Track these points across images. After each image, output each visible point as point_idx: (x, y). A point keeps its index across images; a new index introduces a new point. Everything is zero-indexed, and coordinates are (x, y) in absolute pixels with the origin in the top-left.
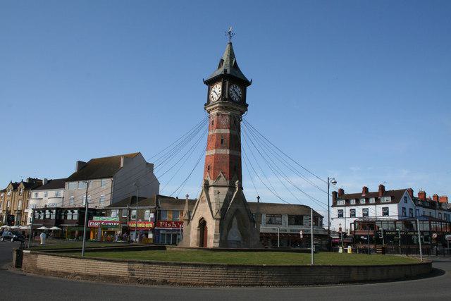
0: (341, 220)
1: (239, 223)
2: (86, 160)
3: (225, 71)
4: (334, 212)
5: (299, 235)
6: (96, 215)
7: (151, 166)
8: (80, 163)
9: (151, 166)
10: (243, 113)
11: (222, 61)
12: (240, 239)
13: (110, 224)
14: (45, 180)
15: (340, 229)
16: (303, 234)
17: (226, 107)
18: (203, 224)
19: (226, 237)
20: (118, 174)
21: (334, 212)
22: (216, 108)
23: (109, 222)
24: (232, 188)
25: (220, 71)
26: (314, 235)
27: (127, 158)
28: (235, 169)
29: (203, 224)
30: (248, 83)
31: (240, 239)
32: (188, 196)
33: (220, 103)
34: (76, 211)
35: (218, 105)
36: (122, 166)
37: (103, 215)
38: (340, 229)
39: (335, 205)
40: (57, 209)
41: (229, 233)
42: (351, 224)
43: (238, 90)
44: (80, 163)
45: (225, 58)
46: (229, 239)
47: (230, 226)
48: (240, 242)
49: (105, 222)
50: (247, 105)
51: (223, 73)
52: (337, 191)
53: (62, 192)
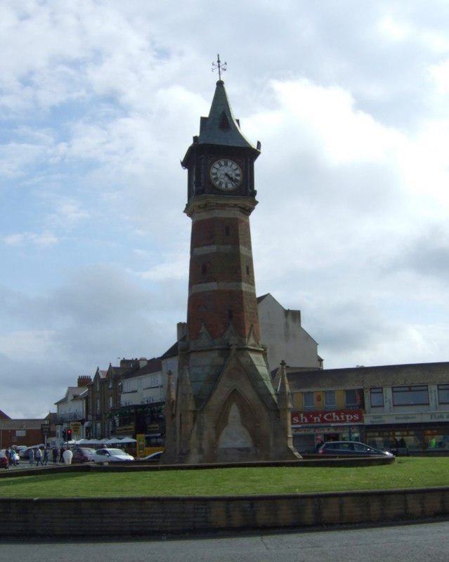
1: (243, 413)
12: (249, 444)
19: (214, 445)
28: (231, 317)
48: (247, 450)
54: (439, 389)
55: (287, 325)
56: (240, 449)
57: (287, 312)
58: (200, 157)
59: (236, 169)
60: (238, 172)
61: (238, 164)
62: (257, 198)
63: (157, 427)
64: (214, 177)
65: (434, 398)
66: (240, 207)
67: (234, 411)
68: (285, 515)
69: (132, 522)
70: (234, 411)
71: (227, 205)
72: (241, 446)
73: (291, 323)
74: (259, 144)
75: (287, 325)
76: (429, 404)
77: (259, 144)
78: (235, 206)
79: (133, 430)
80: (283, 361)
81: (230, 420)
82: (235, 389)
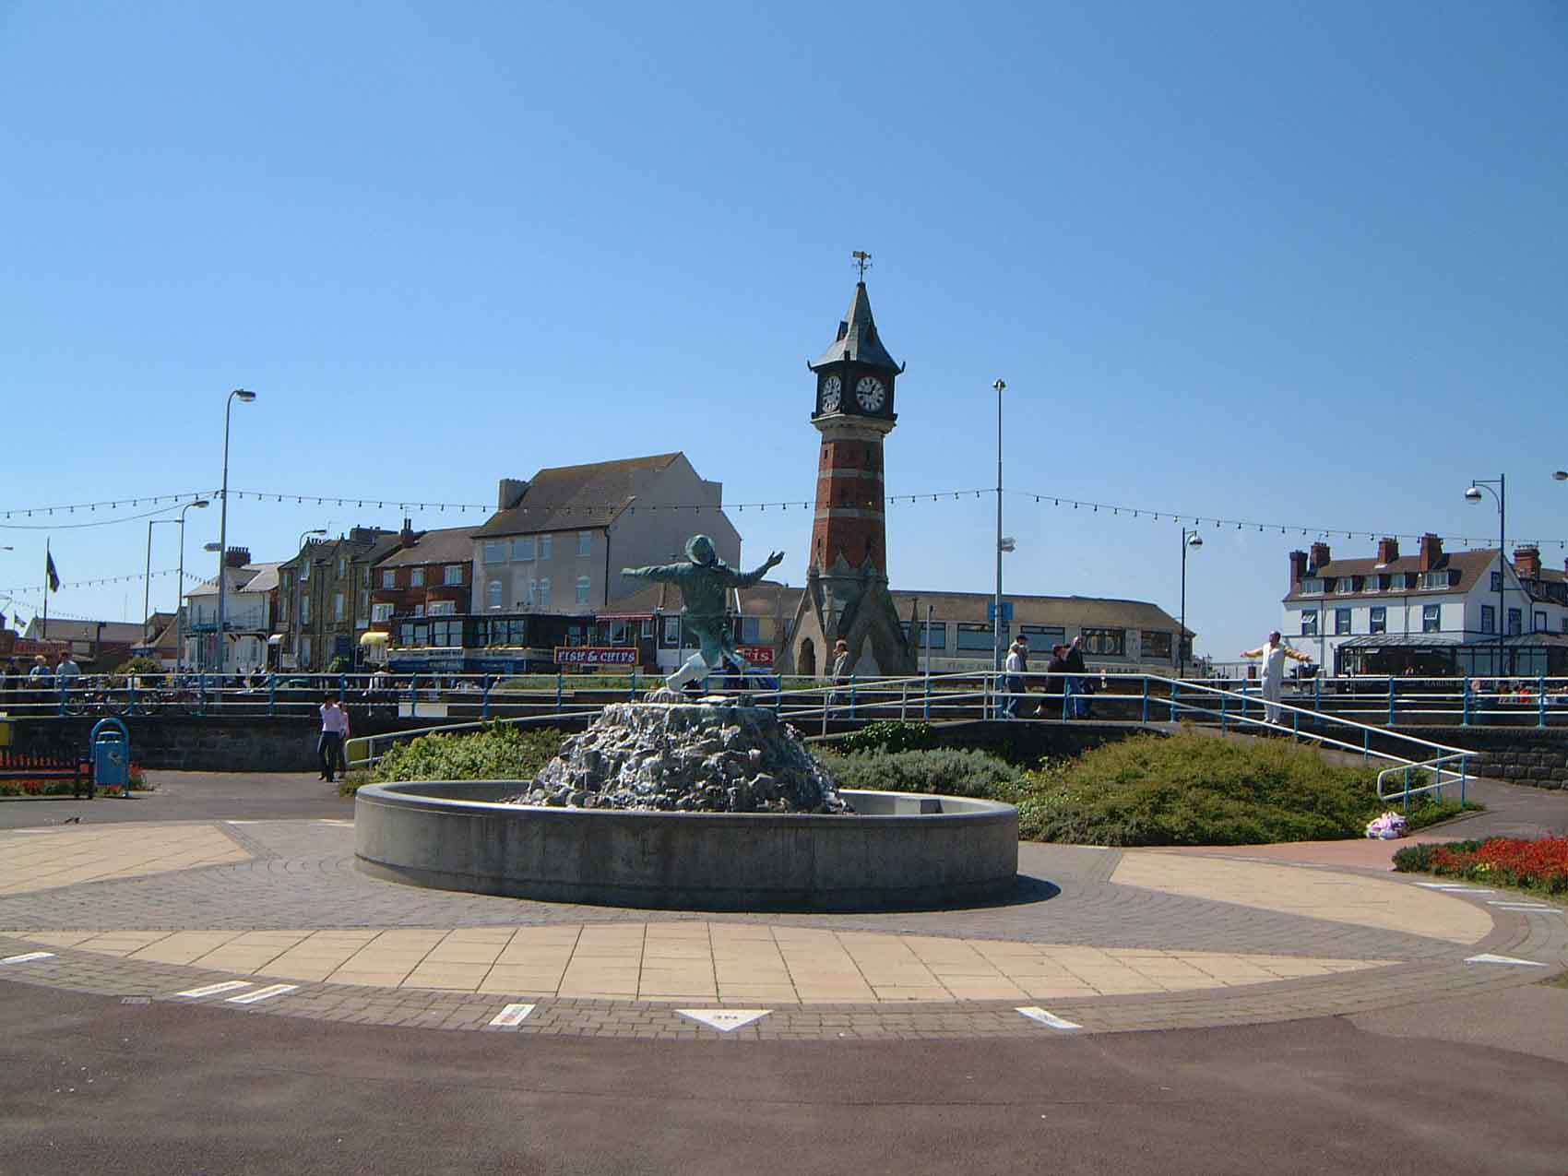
2: (526, 476)
7: (714, 490)
10: (884, 432)
54: (958, 630)
59: (881, 396)
67: (868, 643)
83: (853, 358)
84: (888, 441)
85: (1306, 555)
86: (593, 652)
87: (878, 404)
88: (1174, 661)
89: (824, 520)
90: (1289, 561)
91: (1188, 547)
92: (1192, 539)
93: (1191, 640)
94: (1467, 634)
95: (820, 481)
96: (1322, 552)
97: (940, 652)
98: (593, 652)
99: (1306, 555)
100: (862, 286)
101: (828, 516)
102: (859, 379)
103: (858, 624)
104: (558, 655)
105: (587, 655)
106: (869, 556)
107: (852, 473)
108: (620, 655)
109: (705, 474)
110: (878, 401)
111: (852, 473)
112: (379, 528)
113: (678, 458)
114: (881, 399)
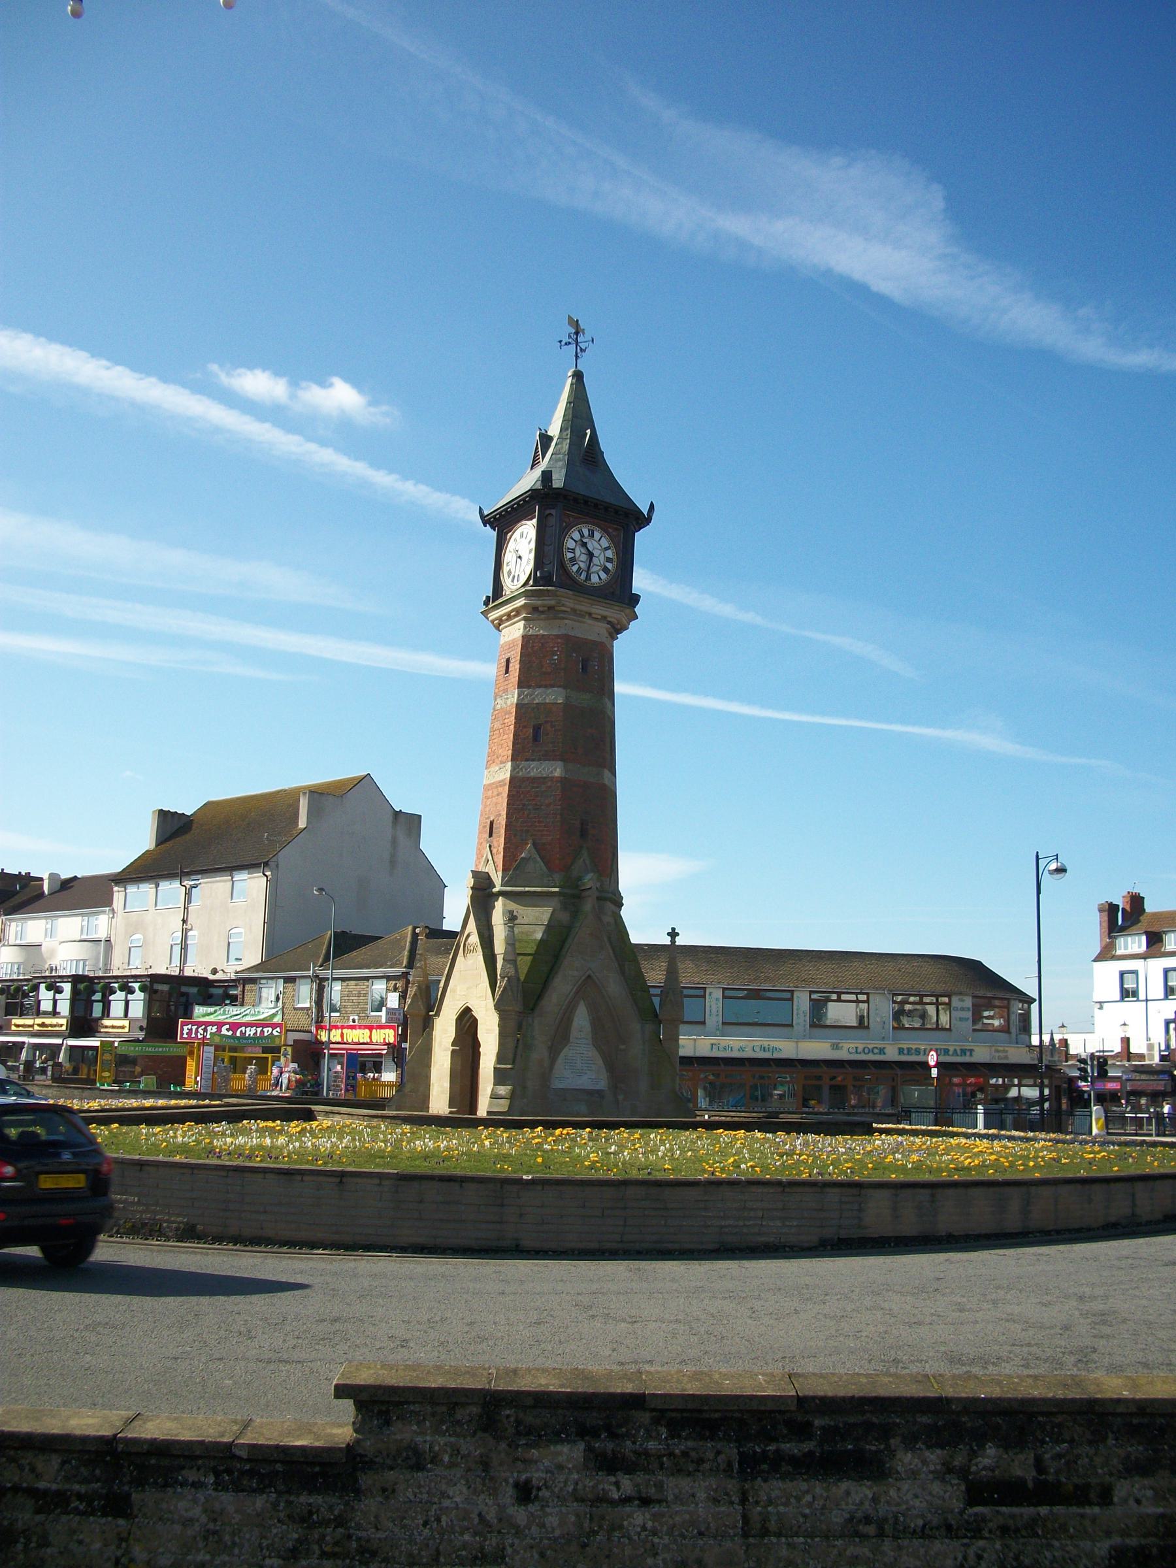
0: (1132, 1009)
1: (597, 1024)
2: (188, 807)
3: (546, 476)
4: (1106, 976)
5: (925, 1066)
6: (207, 1001)
7: (411, 824)
8: (165, 816)
9: (411, 824)
10: (617, 629)
11: (545, 440)
12: (602, 1084)
13: (250, 1032)
14: (53, 877)
15: (1126, 1041)
16: (938, 1065)
17: (551, 608)
18: (467, 1022)
19: (546, 1076)
20: (288, 856)
21: (1106, 976)
22: (518, 611)
23: (247, 1025)
24: (572, 898)
25: (530, 480)
26: (236, 1057)
27: (319, 795)
28: (583, 833)
29: (467, 1022)
30: (641, 520)
31: (602, 1084)
32: (673, 934)
33: (526, 594)
34: (67, 987)
35: (521, 602)
36: (302, 823)
37: (233, 1000)
38: (1126, 1041)
39: (1106, 954)
40: (76, 979)
41: (560, 1061)
42: (1167, 1023)
43: (600, 545)
44: (165, 816)
45: (554, 430)
46: (556, 1084)
47: (561, 1036)
48: (600, 1093)
49: (234, 1026)
50: (635, 599)
51: (539, 486)
52: (1119, 902)
53: (101, 924)
54: (724, 997)
55: (394, 841)
56: (590, 1093)
57: (397, 814)
58: (548, 512)
59: (607, 549)
60: (609, 554)
61: (612, 538)
62: (638, 609)
63: (123, 1027)
64: (570, 555)
65: (714, 1010)
66: (609, 623)
67: (581, 1019)
68: (981, 1215)
69: (722, 1227)
70: (581, 1019)
71: (590, 614)
72: (589, 1086)
73: (402, 839)
74: (652, 506)
75: (394, 841)
76: (704, 1023)
77: (652, 506)
78: (604, 618)
79: (64, 1028)
80: (673, 929)
81: (574, 1033)
82: (589, 976)
83: (558, 482)
84: (623, 648)
85: (1118, 906)
86: (228, 1026)
87: (603, 576)
88: (1014, 1035)
89: (500, 784)
90: (1098, 913)
91: (1046, 879)
92: (1053, 866)
93: (1029, 1008)
94: (975, 1000)
95: (497, 715)
96: (1137, 901)
97: (699, 1027)
98: (228, 1026)
99: (1118, 906)
100: (578, 376)
101: (508, 775)
102: (569, 527)
103: (561, 987)
104: (182, 1030)
105: (219, 1030)
106: (585, 853)
107: (554, 696)
108: (197, 1029)
109: (401, 802)
110: (606, 570)
111: (554, 696)
112: (29, 873)
113: (365, 782)
114: (609, 566)
